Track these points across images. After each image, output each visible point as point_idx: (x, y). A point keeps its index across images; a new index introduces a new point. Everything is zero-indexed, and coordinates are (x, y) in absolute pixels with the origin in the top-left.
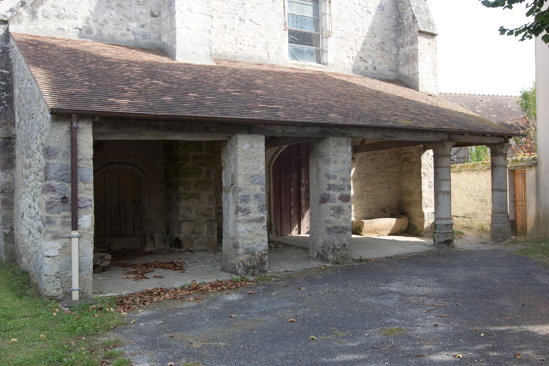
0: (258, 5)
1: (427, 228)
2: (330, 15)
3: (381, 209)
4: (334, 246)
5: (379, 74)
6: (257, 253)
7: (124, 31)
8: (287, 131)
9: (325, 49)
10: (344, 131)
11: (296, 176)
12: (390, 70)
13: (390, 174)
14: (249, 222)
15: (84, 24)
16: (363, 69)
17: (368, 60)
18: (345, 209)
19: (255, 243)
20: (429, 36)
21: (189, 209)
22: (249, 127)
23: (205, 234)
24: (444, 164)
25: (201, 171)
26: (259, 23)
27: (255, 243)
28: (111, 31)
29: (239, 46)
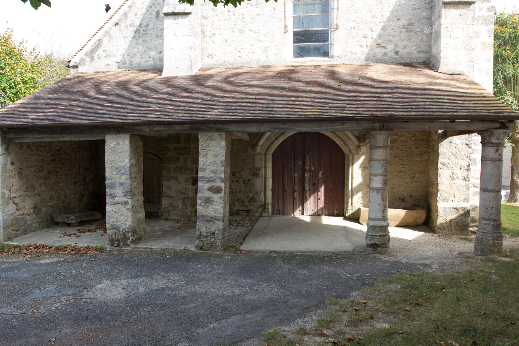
0: (258, 16)
1: (442, 224)
2: (338, 8)
3: (400, 198)
4: (201, 232)
6: (121, 230)
7: (147, 59)
8: (155, 129)
9: (332, 43)
10: (219, 126)
11: (300, 162)
12: (418, 52)
13: (414, 163)
14: (114, 204)
15: (122, 59)
16: (391, 54)
18: (215, 199)
19: (119, 221)
20: (461, 6)
21: (169, 188)
22: (118, 128)
23: (180, 208)
25: (179, 159)
26: (259, 31)
27: (119, 221)
28: (138, 61)
29: (239, 54)
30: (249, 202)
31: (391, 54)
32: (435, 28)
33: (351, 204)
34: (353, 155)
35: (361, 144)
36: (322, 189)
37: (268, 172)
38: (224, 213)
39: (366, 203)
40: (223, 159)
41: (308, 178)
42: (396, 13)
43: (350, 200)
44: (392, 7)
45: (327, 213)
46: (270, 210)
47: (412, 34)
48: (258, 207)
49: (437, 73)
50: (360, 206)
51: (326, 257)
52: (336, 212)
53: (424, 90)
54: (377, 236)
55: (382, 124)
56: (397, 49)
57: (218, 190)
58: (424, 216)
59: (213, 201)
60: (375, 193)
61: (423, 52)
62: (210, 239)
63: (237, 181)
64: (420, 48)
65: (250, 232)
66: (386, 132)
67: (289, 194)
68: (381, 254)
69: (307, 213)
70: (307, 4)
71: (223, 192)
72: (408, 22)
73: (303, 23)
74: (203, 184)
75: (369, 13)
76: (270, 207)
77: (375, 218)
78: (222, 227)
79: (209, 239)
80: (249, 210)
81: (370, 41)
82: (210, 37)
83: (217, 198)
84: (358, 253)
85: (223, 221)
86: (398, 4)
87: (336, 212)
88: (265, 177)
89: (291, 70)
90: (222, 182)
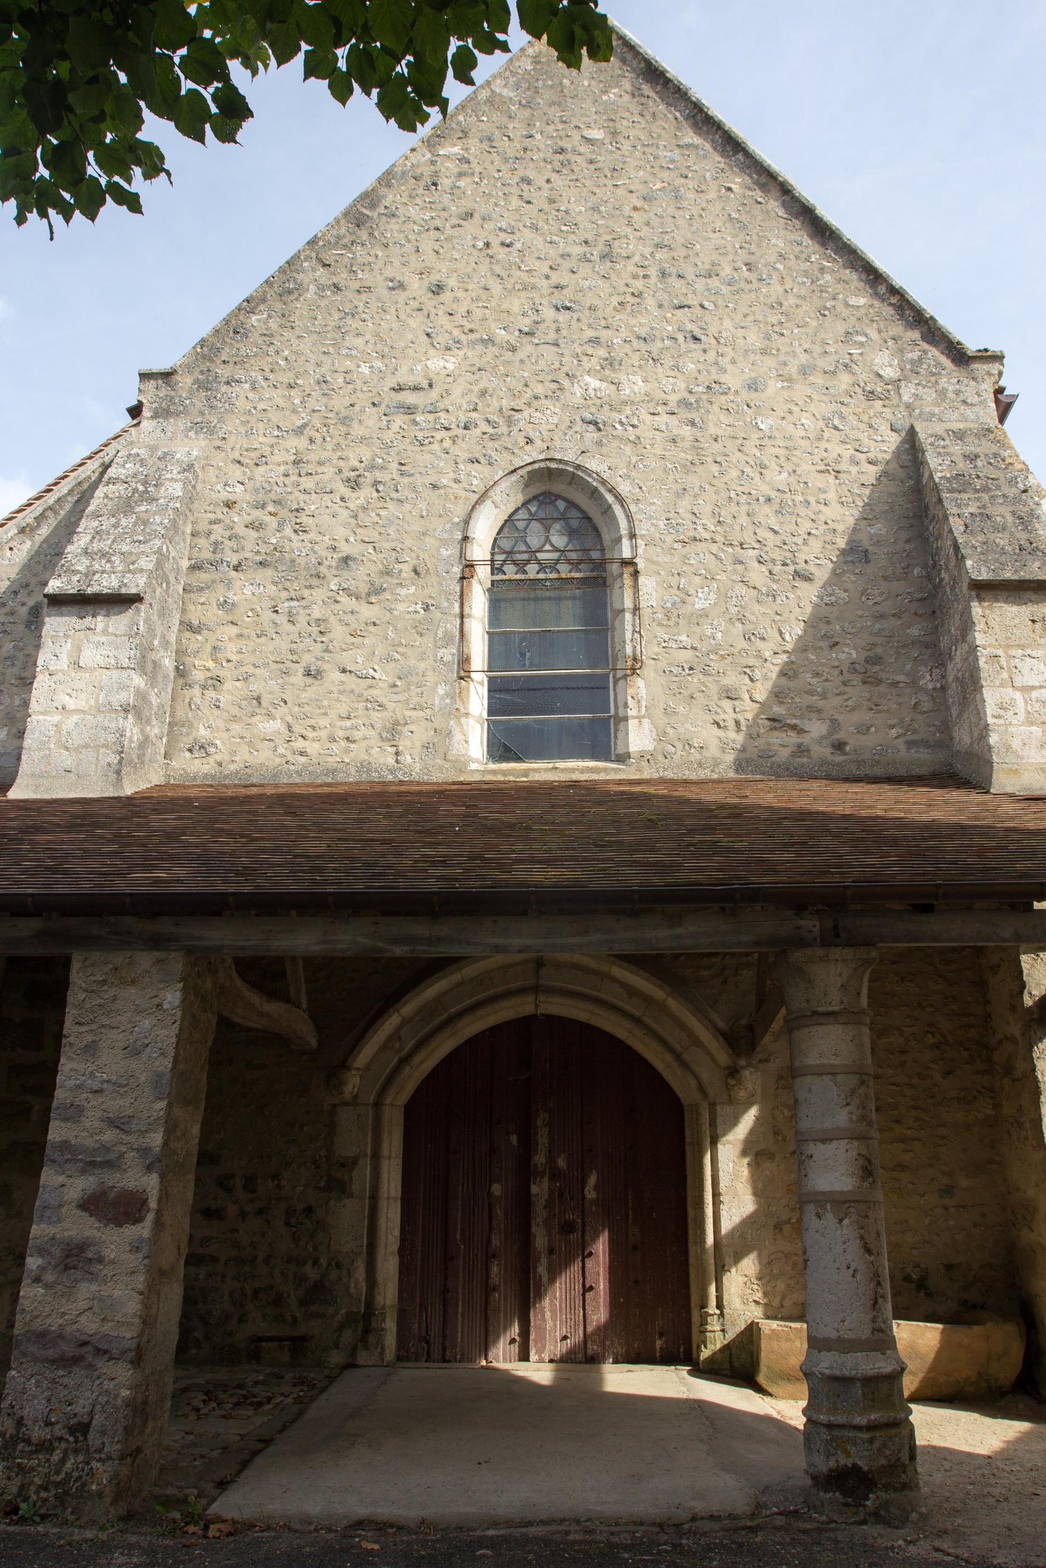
0: (371, 628)
2: (636, 609)
3: (907, 1278)
5: (859, 763)
9: (621, 714)
10: (164, 926)
11: (514, 1139)
12: (910, 744)
16: (822, 752)
17: (806, 725)
18: (110, 1253)
20: (1028, 595)
24: (812, 1060)
29: (300, 744)
30: (304, 1302)
31: (822, 752)
32: (954, 667)
33: (720, 1306)
34: (713, 1105)
35: (742, 1062)
36: (601, 1247)
37: (384, 1176)
38: (148, 1321)
39: (776, 1303)
40: (165, 1064)
41: (542, 1202)
42: (824, 628)
43: (712, 1289)
44: (809, 609)
45: (621, 1350)
46: (390, 1340)
47: (882, 688)
48: (342, 1327)
49: (988, 797)
50: (755, 1313)
51: (628, 1548)
52: (659, 1343)
53: (960, 830)
54: (858, 1428)
55: (829, 924)
56: (840, 736)
57: (123, 1209)
58: (1017, 1351)
59: (100, 1260)
60: (830, 1218)
61: (925, 743)
62: (63, 1461)
63: (261, 1212)
64: (915, 731)
65: (284, 1428)
66: (848, 953)
67: (471, 1274)
68: (888, 1524)
69: (540, 1352)
70: (536, 599)
71: (150, 1217)
72: (864, 654)
73: (523, 655)
74: (61, 1179)
75: (738, 625)
76: (390, 1325)
77: (840, 1340)
78: (125, 1393)
79: (56, 1457)
80: (303, 1339)
81: (748, 711)
82: (204, 687)
83: (117, 1243)
84: (780, 1521)
85: (137, 1362)
86: (827, 600)
87: (659, 1343)
88: (374, 1198)
89: (480, 790)
90: (149, 1168)
